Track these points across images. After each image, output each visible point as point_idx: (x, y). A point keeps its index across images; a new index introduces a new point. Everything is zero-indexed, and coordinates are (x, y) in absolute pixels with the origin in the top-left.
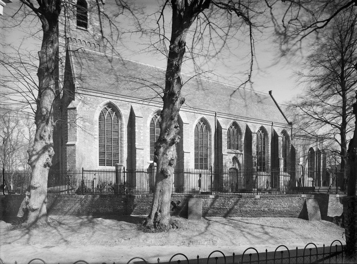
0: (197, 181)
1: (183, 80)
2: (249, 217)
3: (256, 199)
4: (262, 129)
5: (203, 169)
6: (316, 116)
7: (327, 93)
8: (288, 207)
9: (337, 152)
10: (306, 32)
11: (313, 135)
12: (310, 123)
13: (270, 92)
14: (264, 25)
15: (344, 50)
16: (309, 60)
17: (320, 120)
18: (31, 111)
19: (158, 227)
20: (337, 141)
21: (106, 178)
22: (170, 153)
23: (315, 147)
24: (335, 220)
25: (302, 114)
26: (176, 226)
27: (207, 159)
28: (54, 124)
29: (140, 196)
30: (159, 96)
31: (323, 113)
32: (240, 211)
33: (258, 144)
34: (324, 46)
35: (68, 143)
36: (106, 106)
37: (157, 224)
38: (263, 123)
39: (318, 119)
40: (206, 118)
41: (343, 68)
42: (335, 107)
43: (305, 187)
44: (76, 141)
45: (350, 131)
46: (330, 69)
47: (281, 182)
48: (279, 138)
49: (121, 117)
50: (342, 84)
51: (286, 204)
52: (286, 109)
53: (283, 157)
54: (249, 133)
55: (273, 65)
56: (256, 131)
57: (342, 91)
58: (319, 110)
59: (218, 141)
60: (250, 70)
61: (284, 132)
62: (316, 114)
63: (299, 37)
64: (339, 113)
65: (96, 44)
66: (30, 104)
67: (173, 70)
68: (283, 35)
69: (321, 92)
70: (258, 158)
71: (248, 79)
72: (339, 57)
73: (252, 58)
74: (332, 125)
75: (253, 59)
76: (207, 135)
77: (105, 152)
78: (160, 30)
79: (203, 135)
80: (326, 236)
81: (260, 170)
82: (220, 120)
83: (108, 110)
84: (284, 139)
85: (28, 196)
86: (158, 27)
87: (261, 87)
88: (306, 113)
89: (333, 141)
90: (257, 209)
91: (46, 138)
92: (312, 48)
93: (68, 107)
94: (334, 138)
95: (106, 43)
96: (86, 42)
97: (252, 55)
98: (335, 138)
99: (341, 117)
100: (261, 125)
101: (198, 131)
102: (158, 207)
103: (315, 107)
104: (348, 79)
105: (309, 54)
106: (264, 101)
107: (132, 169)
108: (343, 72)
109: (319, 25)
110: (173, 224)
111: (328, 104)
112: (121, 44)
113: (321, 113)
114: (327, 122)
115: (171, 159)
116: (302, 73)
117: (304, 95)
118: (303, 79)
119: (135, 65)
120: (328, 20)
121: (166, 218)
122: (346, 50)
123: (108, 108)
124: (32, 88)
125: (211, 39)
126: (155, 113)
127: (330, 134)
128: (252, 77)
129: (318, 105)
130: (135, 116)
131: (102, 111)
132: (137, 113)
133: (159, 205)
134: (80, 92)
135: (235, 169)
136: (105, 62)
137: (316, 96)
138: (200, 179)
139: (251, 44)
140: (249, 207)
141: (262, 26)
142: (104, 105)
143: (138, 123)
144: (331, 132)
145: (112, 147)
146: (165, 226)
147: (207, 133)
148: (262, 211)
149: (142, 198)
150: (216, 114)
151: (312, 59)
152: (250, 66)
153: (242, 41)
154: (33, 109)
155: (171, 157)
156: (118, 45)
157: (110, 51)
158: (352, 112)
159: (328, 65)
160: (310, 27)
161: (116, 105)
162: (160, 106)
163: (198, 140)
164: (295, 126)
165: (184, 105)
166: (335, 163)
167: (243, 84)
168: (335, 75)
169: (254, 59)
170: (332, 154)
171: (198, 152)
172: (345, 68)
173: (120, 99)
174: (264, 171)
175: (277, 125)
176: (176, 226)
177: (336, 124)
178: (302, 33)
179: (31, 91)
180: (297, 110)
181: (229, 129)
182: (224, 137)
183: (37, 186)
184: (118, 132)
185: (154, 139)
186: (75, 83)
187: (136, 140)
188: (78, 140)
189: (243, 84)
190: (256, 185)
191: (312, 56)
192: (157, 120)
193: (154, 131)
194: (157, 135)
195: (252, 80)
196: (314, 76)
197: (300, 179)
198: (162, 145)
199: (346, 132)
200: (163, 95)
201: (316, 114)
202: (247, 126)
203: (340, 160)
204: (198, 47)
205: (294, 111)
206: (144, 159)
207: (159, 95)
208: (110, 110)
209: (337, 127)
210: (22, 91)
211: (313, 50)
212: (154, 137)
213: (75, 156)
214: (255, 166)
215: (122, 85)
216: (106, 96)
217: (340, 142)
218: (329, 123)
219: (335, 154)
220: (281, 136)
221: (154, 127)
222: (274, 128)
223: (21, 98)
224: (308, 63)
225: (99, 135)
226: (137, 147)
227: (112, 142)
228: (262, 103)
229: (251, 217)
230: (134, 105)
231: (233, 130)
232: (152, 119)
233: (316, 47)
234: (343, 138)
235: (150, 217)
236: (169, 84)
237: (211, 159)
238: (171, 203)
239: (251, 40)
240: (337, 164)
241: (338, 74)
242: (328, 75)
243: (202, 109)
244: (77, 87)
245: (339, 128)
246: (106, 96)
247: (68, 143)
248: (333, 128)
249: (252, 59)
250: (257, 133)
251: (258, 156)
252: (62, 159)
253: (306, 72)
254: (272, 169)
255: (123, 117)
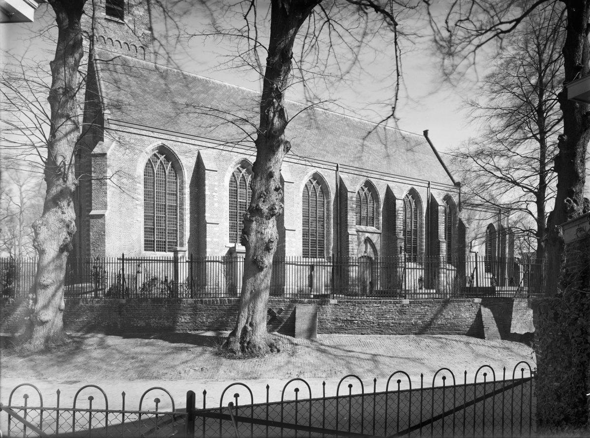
0: (307, 276)
1: (289, 113)
2: (392, 334)
3: (403, 306)
4: (413, 193)
5: (308, 257)
6: (498, 174)
7: (516, 136)
8: (453, 319)
9: (531, 232)
10: (483, 38)
11: (494, 204)
12: (489, 184)
13: (426, 133)
14: (417, 32)
15: (543, 68)
16: (487, 82)
17: (504, 179)
18: (39, 160)
19: (249, 350)
20: (531, 213)
21: (156, 271)
22: (267, 230)
23: (497, 223)
24: (525, 339)
25: (476, 169)
26: (276, 348)
27: (323, 241)
28: (77, 182)
29: (217, 301)
30: (249, 139)
31: (510, 168)
32: (378, 325)
33: (406, 218)
34: (512, 59)
35: (93, 213)
36: (156, 152)
37: (246, 345)
38: (414, 183)
39: (501, 178)
40: (321, 172)
41: (541, 96)
42: (528, 159)
43: (480, 288)
44: (106, 209)
45: (551, 198)
46: (521, 97)
47: (442, 279)
48: (439, 208)
49: (181, 170)
50: (541, 122)
51: (451, 313)
52: (451, 161)
53: (445, 239)
54: (390, 197)
55: (430, 94)
56: (403, 196)
57: (540, 133)
58: (503, 162)
59: (340, 213)
60: (394, 99)
61: (447, 199)
62: (498, 169)
63: (472, 48)
64: (534, 168)
65: (137, 46)
66: (36, 147)
67: (271, 95)
68: (446, 47)
69: (505, 135)
70: (405, 240)
71: (391, 113)
72: (534, 81)
73: (398, 79)
74: (523, 187)
75: (400, 81)
76: (324, 202)
77: (154, 229)
78: (249, 30)
79: (316, 200)
80: (509, 362)
81: (409, 260)
82: (343, 176)
83: (159, 159)
84: (448, 210)
85: (33, 299)
86: (246, 24)
87: (411, 125)
88: (483, 167)
89: (525, 214)
90: (404, 322)
91: (62, 205)
92: (494, 62)
93: (93, 153)
94: (527, 209)
95: (156, 48)
96: (122, 42)
97: (398, 75)
98: (529, 209)
99: (538, 176)
100: (410, 187)
101: (308, 194)
102: (248, 319)
103: (496, 159)
104: (549, 114)
105: (488, 72)
106: (414, 149)
107: (198, 259)
108: (541, 103)
109: (504, 27)
110: (272, 348)
111: (518, 154)
112: (183, 51)
113: (506, 169)
114: (515, 183)
115: (269, 240)
116: (477, 102)
117: (479, 140)
118: (479, 112)
119: (205, 84)
120: (518, 21)
121: (261, 334)
122: (546, 67)
123: (159, 155)
124: (41, 122)
125: (331, 46)
126: (238, 164)
127: (519, 203)
128: (396, 109)
129: (503, 156)
130: (204, 169)
131: (149, 160)
132: (207, 164)
133: (249, 314)
134: (113, 127)
135: (369, 258)
136: (154, 78)
137: (499, 141)
138: (311, 274)
139: (397, 57)
140: (393, 318)
141: (415, 34)
142: (153, 150)
143: (210, 180)
144: (521, 200)
145: (165, 220)
146: (259, 348)
147: (324, 199)
148: (412, 324)
149: (221, 303)
150: (337, 167)
151: (493, 80)
152: (394, 93)
153: (382, 52)
154: (41, 157)
155: (270, 237)
156: (177, 52)
157: (165, 62)
158: (553, 169)
159: (517, 91)
160: (490, 30)
161: (173, 149)
162: (252, 153)
163: (309, 209)
164: (464, 189)
165: (290, 152)
166: (529, 249)
167: (384, 120)
168: (529, 107)
169: (400, 81)
170: (523, 234)
171: (309, 230)
172: (544, 96)
173: (180, 139)
174: (415, 261)
175: (437, 187)
176: (276, 348)
177: (529, 187)
178: (476, 41)
179: (38, 126)
180: (468, 163)
181: (358, 192)
182: (352, 204)
183: (49, 283)
184: (176, 195)
185: (236, 207)
186: (105, 112)
187: (207, 209)
188: (109, 208)
189: (384, 120)
190: (404, 283)
191: (493, 75)
192: (241, 176)
193: (236, 193)
194: (241, 201)
195: (397, 114)
196: (495, 109)
197: (472, 276)
198: (254, 219)
199: (546, 199)
200: (255, 137)
201: (498, 169)
202: (388, 188)
203: (537, 244)
204: (310, 59)
205: (464, 164)
206: (219, 240)
207: (249, 137)
208: (162, 158)
209: (531, 191)
210: (24, 127)
211: (495, 65)
212: (237, 204)
213: (105, 235)
214: (401, 253)
215: (183, 118)
216: (156, 135)
217: (536, 215)
218: (518, 184)
219: (528, 235)
220: (443, 204)
221: (236, 187)
222: (432, 191)
223: (23, 139)
224: (486, 87)
225: (145, 200)
226: (208, 220)
227: (165, 211)
228: (412, 151)
229: (395, 334)
230: (204, 154)
231: (365, 193)
232: (233, 173)
233: (500, 62)
234: (541, 209)
235: (233, 334)
236: (265, 121)
237: (328, 240)
238: (268, 312)
239: (396, 51)
240: (532, 251)
241: (534, 106)
242: (519, 107)
243: (316, 158)
244: (108, 119)
245: (535, 193)
246: (156, 135)
247: (93, 213)
248: (525, 193)
249: (398, 81)
250: (404, 200)
251: (405, 238)
252: (80, 239)
253: (483, 101)
254: (427, 259)
255: (185, 170)
